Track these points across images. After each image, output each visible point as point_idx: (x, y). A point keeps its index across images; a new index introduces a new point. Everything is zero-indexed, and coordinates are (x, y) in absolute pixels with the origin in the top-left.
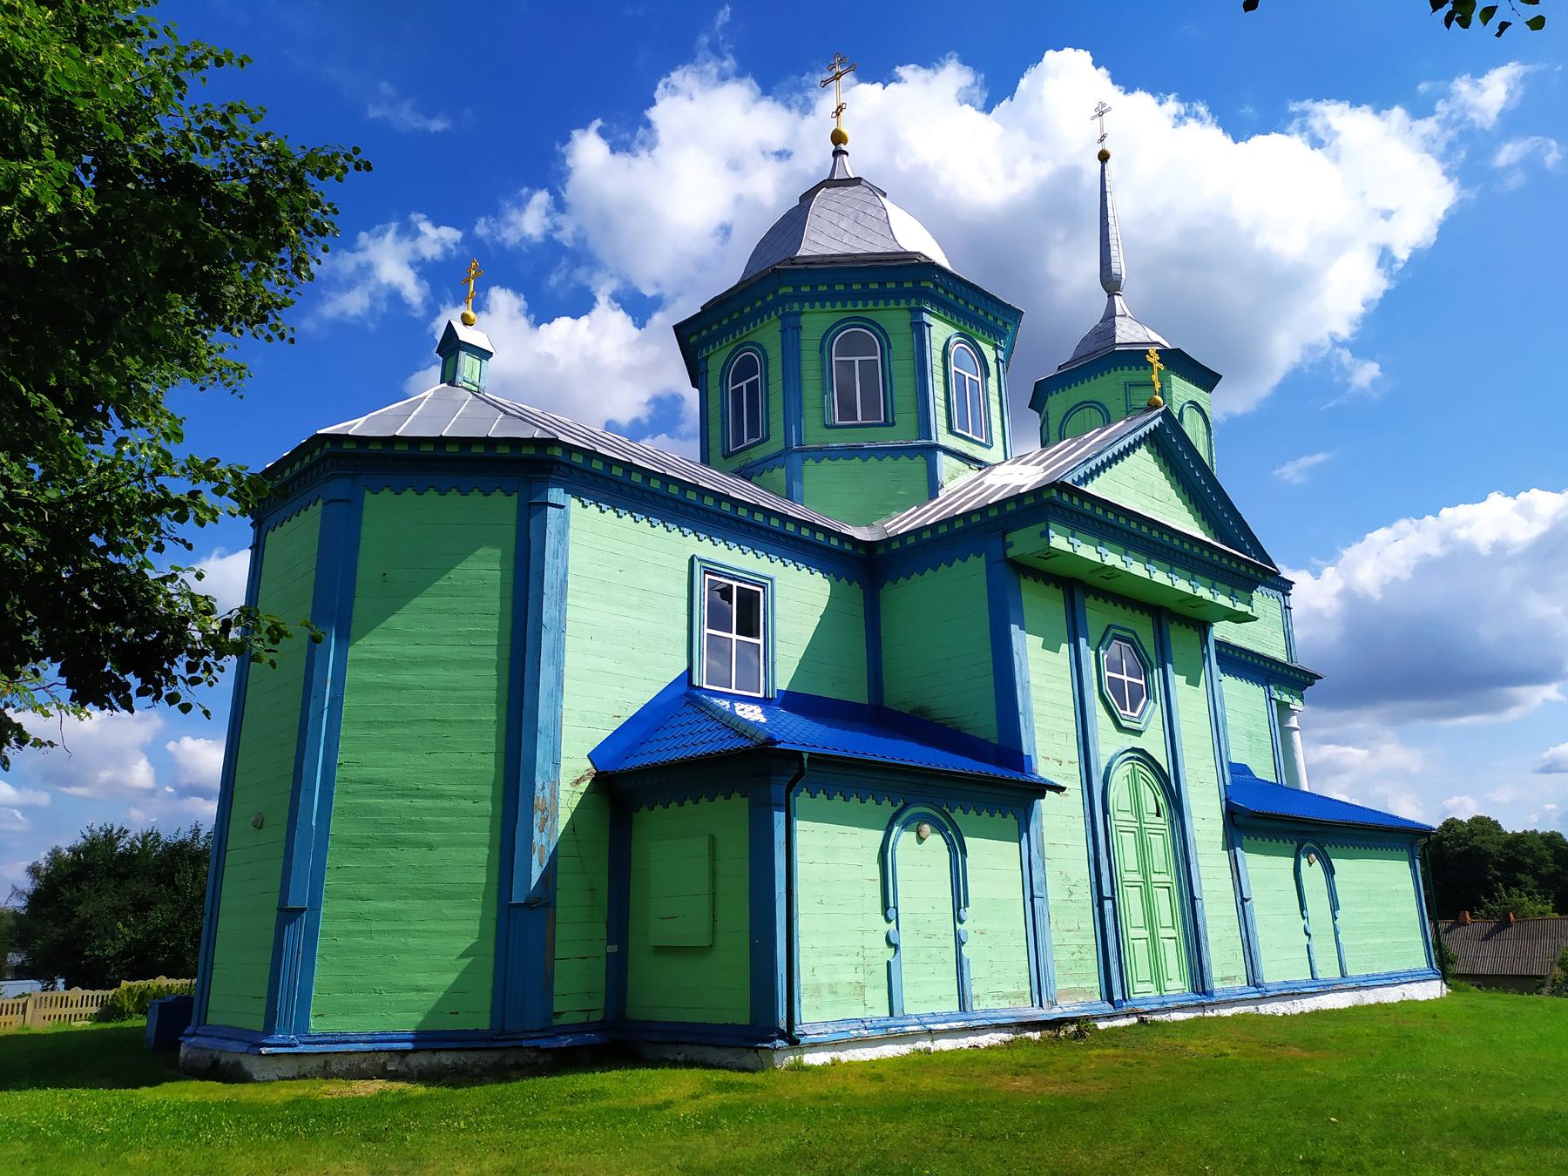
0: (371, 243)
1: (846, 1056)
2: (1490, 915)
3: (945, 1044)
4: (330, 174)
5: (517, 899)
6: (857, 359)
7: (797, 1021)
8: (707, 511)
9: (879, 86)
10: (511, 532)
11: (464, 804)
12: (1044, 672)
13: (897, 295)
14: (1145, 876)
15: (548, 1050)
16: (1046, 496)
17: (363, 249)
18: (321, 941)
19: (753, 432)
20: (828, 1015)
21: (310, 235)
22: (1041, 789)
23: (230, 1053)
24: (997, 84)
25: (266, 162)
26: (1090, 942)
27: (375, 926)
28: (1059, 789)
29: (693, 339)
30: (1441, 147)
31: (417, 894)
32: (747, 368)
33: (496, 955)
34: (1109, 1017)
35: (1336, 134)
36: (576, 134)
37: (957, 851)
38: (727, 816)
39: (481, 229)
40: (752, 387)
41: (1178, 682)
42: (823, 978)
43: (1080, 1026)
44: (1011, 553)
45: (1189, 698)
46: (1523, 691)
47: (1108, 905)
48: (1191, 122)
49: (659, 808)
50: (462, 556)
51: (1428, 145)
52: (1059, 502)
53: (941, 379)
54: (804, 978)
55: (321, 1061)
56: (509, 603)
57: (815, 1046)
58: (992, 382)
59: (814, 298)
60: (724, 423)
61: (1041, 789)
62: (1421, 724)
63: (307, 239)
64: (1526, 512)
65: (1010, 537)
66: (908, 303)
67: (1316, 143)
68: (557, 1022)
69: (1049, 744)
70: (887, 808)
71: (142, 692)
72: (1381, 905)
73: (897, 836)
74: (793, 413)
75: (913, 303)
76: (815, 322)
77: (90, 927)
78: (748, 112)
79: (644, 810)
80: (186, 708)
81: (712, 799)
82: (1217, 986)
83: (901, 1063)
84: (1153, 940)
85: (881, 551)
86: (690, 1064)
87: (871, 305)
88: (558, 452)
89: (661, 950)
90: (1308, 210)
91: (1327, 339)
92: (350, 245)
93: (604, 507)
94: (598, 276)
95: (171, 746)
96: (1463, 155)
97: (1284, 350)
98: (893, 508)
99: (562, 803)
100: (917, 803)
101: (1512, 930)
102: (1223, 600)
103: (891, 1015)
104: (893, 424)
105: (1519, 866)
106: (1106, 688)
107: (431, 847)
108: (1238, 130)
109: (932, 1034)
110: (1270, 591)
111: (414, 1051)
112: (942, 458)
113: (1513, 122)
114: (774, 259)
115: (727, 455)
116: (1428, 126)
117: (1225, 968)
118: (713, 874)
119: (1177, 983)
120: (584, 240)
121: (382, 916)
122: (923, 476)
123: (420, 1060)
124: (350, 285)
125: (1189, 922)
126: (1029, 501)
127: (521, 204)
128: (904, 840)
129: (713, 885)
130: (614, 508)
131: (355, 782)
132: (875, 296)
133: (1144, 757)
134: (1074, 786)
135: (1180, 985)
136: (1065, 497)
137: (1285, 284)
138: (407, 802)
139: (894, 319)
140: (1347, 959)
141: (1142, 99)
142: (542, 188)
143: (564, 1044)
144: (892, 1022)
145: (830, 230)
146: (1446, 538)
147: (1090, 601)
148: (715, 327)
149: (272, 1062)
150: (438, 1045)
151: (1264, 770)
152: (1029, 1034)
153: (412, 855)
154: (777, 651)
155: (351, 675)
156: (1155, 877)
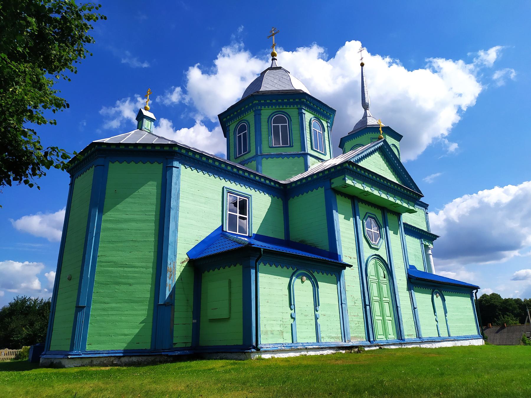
0: (121, 104)
1: (276, 356)
2: (498, 324)
3: (312, 353)
4: (92, 19)
5: (161, 302)
6: (280, 125)
7: (259, 343)
8: (228, 171)
9: (291, 52)
10: (160, 176)
11: (142, 269)
12: (345, 227)
13: (293, 104)
14: (380, 298)
15: (171, 356)
16: (344, 166)
17: (118, 107)
18: (91, 318)
19: (245, 150)
20: (271, 341)
21: (84, 42)
22: (345, 266)
23: (56, 359)
24: (330, 53)
25: (68, 8)
26: (362, 320)
27: (110, 313)
28: (350, 266)
29: (224, 120)
30: (475, 73)
31: (126, 301)
32: (243, 128)
33: (153, 322)
34: (369, 346)
35: (441, 68)
36: (190, 68)
37: (315, 286)
38: (235, 272)
39: (158, 100)
40: (245, 135)
41: (391, 233)
42: (269, 328)
43: (359, 348)
44: (333, 186)
45: (395, 239)
46: (506, 253)
47: (368, 307)
48: (394, 65)
49: (211, 271)
50: (143, 185)
51: (471, 72)
52: (349, 168)
53: (309, 132)
54: (262, 328)
55: (90, 360)
56: (159, 200)
57: (266, 352)
58: (326, 133)
59: (265, 104)
60: (235, 147)
61: (345, 266)
62: (474, 264)
63: (83, 43)
64: (506, 192)
65: (332, 181)
66: (297, 106)
67: (434, 71)
68: (174, 347)
69: (347, 251)
70: (291, 271)
71: (15, 179)
72: (461, 314)
73: (294, 280)
74: (259, 142)
75: (299, 106)
76: (266, 113)
77: (14, 332)
78: (247, 61)
79: (206, 272)
80: (31, 186)
81: (230, 267)
82: (406, 337)
83: (296, 358)
84: (384, 321)
85: (289, 187)
86: (221, 359)
87: (285, 107)
88: (177, 149)
89: (212, 321)
90: (432, 95)
91: (440, 136)
92: (114, 105)
93: (193, 169)
94: (197, 115)
95: (46, 274)
96: (482, 75)
97: (426, 139)
98: (292, 174)
99: (177, 270)
100: (301, 269)
101: (505, 330)
102: (405, 205)
103: (293, 342)
104: (293, 146)
105: (508, 310)
106: (366, 234)
107: (130, 285)
108: (410, 68)
109: (307, 349)
110: (421, 208)
111: (123, 356)
112: (310, 158)
113: (499, 64)
114: (251, 93)
115: (236, 158)
116: (471, 66)
117: (409, 332)
118: (230, 293)
119: (392, 336)
120: (193, 104)
121: (112, 309)
122: (303, 164)
123: (126, 359)
124: (113, 118)
125: (396, 314)
126: (339, 168)
127: (172, 92)
128: (297, 282)
129: (230, 296)
130: (196, 169)
131: (104, 262)
132: (286, 104)
133: (379, 257)
134: (356, 266)
135: (393, 337)
136: (351, 166)
137: (427, 118)
138: (122, 269)
139: (293, 111)
140: (450, 331)
141: (378, 58)
142: (178, 86)
143: (177, 354)
144: (293, 345)
145: (271, 83)
146: (481, 202)
147: (360, 204)
148: (232, 115)
149: (72, 361)
150: (132, 354)
151: (420, 267)
152: (341, 351)
153: (123, 288)
154: (253, 220)
155: (103, 225)
156: (384, 299)
